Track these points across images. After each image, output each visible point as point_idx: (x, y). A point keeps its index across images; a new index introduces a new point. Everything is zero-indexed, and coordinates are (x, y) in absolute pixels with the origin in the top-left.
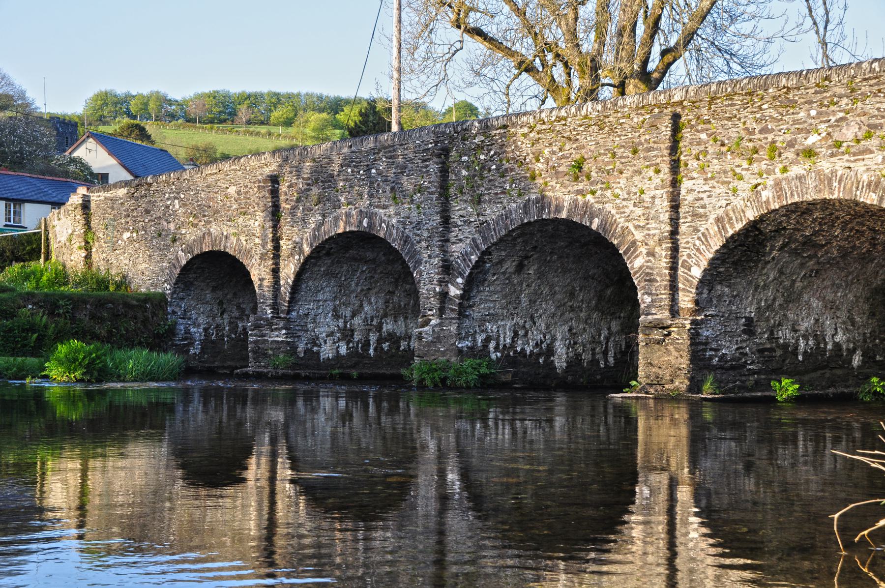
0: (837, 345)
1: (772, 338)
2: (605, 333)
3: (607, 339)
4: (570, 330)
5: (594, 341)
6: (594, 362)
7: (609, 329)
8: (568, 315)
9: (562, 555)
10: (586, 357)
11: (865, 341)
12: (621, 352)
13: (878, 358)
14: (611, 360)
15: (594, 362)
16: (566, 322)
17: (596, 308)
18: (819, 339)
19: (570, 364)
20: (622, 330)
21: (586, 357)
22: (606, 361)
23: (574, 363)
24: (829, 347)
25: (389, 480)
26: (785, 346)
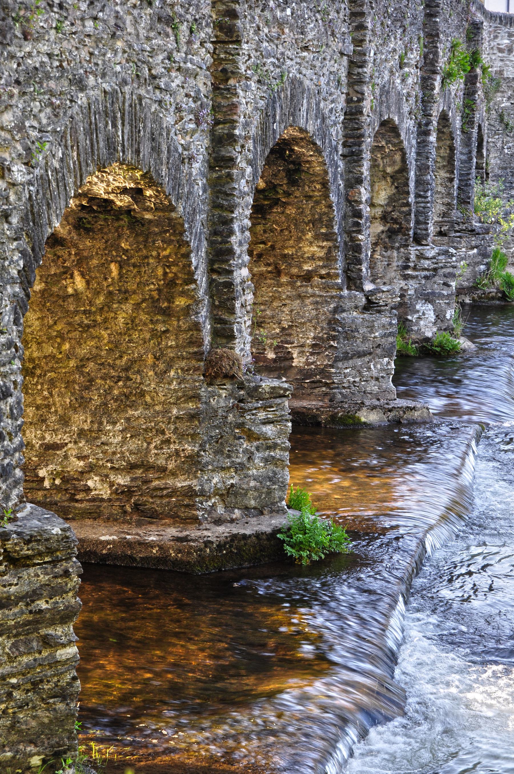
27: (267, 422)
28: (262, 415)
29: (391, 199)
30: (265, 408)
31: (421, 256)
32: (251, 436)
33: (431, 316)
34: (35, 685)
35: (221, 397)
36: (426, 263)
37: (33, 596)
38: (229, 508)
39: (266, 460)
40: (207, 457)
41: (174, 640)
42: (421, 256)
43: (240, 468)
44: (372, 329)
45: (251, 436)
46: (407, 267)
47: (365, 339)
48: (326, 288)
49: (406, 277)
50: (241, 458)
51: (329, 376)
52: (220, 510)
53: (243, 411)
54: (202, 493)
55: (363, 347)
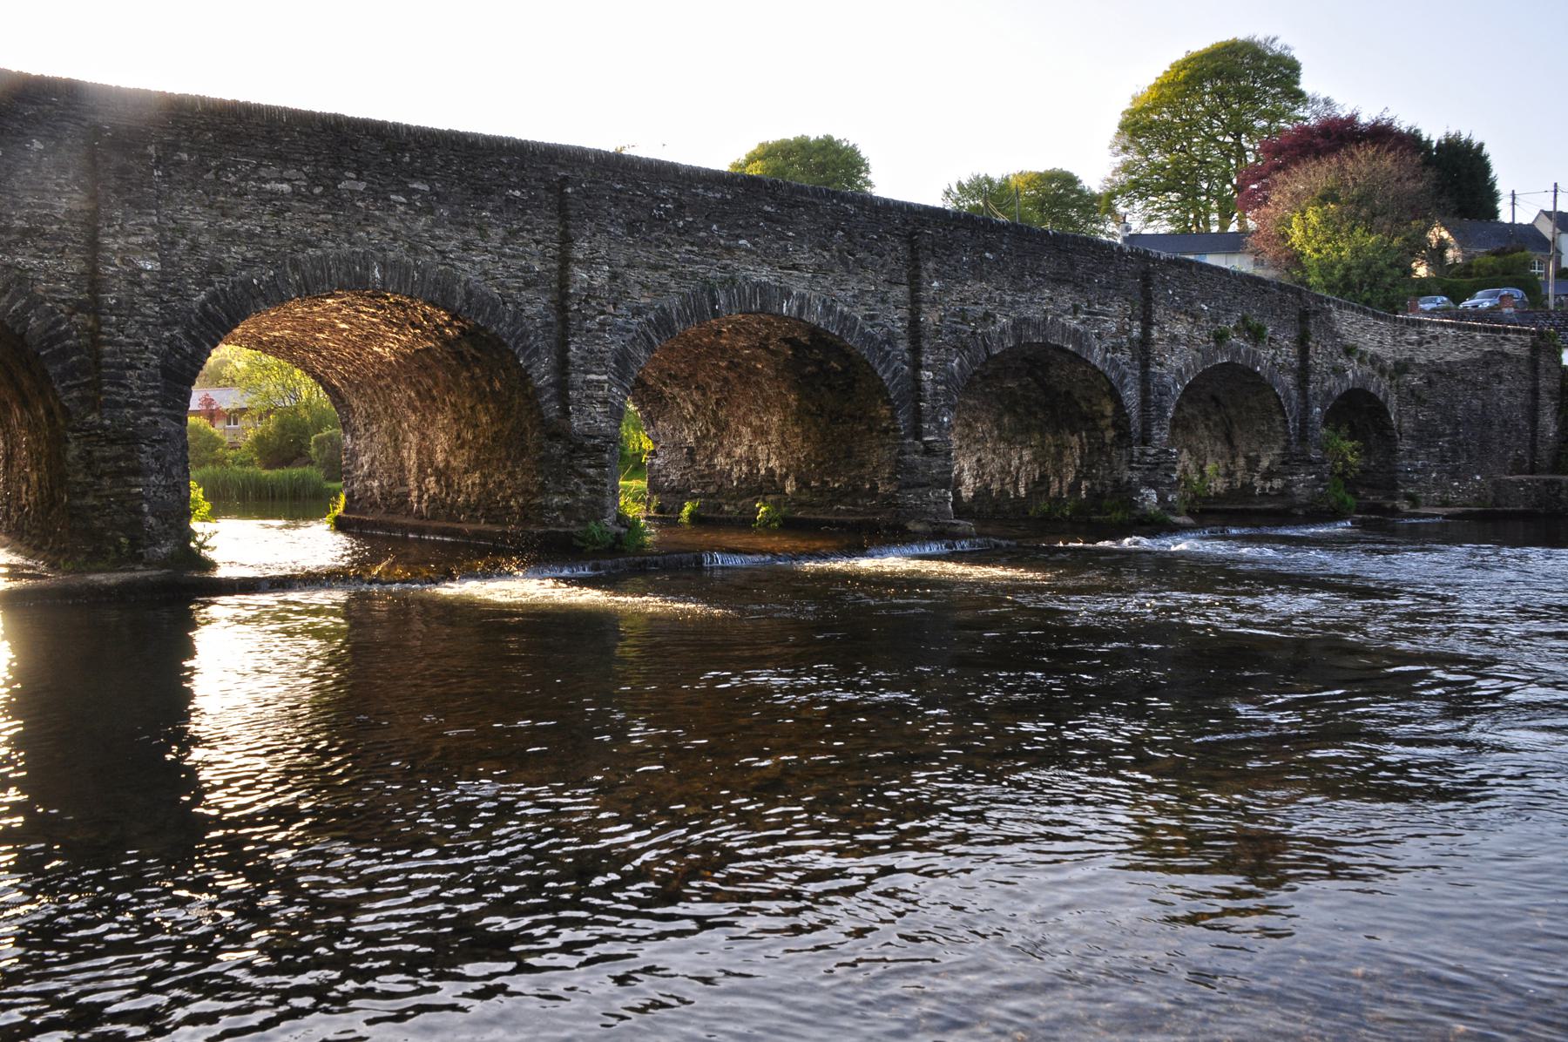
0: (770, 471)
1: (711, 466)
2: (1015, 462)
3: (1018, 469)
4: (979, 460)
5: (1004, 471)
6: (1003, 492)
7: (1020, 458)
8: (974, 447)
9: (1338, 692)
10: (995, 486)
11: (799, 466)
12: (1034, 482)
13: (813, 483)
14: (1022, 491)
15: (1003, 492)
16: (973, 453)
17: (1001, 438)
18: (752, 463)
19: (977, 494)
20: (1035, 460)
21: (995, 486)
22: (1017, 490)
23: (982, 494)
24: (763, 472)
25: (413, 876)
26: (722, 472)
27: (590, 466)
28: (586, 461)
29: (1114, 411)
30: (588, 457)
31: (1143, 454)
32: (581, 475)
33: (1155, 498)
34: (123, 502)
35: (558, 449)
36: (1148, 459)
37: (117, 458)
38: (568, 519)
39: (590, 491)
40: (550, 485)
41: (132, 479)
42: (1143, 454)
43: (572, 494)
44: (930, 467)
45: (581, 475)
46: (1131, 461)
47: (924, 475)
48: (895, 438)
49: (1132, 469)
50: (572, 487)
51: (895, 498)
52: (562, 520)
53: (571, 459)
54: (546, 507)
55: (924, 480)
